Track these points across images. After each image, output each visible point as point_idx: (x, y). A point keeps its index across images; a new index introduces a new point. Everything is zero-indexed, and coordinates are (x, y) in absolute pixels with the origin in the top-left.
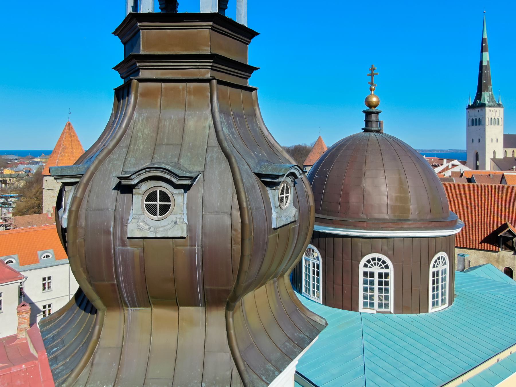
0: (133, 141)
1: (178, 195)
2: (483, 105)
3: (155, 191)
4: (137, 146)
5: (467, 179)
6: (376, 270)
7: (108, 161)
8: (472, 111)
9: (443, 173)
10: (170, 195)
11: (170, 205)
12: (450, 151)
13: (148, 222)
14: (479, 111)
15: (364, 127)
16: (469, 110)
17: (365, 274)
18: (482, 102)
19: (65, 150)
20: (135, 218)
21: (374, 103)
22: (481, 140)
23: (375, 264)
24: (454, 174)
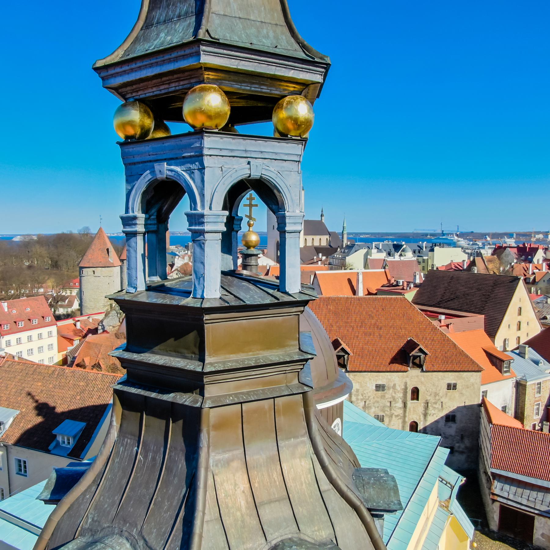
5: (275, 277)
19: (90, 534)
21: (254, 242)
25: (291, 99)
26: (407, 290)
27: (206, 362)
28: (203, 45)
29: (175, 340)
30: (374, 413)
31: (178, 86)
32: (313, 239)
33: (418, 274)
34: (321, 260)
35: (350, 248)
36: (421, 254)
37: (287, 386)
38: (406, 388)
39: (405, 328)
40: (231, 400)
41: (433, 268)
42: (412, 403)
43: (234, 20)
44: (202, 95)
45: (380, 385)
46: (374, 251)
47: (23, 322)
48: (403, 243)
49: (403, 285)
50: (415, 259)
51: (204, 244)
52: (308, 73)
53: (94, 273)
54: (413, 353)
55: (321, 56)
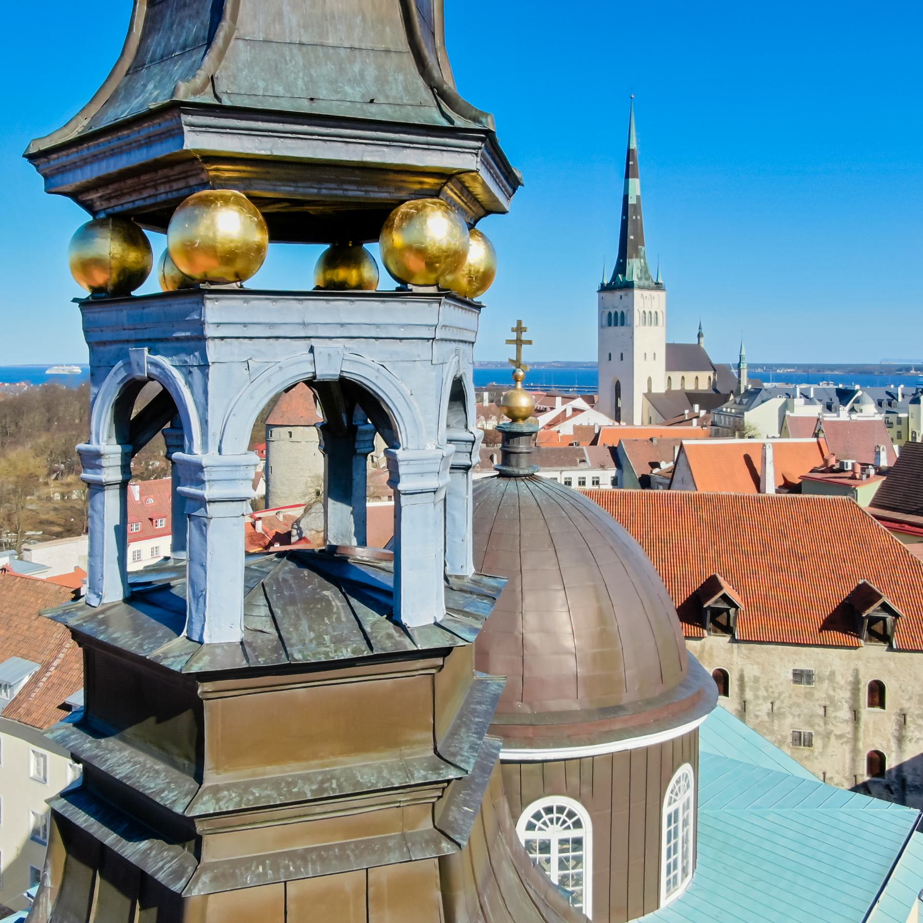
2: (629, 286)
5: (609, 448)
6: (554, 834)
8: (606, 295)
9: (555, 429)
12: (556, 364)
14: (621, 297)
16: (604, 294)
18: (627, 279)
22: (626, 356)
23: (551, 820)
24: (580, 432)
25: (411, 208)
26: (861, 479)
27: (206, 784)
28: (187, 113)
29: (159, 721)
30: (792, 728)
31: (171, 191)
32: (683, 378)
33: (883, 450)
34: (697, 417)
35: (753, 396)
36: (894, 407)
37: (403, 835)
38: (856, 684)
39: (852, 561)
40: (259, 875)
41: (915, 438)
42: (869, 712)
43: (286, 50)
44: (197, 216)
45: (802, 671)
46: (799, 401)
47: (164, 519)
48: (857, 387)
49: (853, 470)
50: (881, 419)
51: (205, 525)
52: (445, 153)
53: (291, 436)
54: (870, 611)
55: (474, 113)
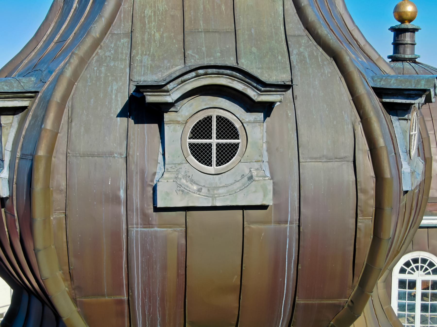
0: (138, 25)
1: (254, 125)
3: (208, 117)
4: (147, 34)
7: (95, 62)
10: (238, 125)
11: (238, 144)
13: (195, 178)
15: (391, 53)
17: (402, 284)
20: (169, 170)
21: (409, 14)
